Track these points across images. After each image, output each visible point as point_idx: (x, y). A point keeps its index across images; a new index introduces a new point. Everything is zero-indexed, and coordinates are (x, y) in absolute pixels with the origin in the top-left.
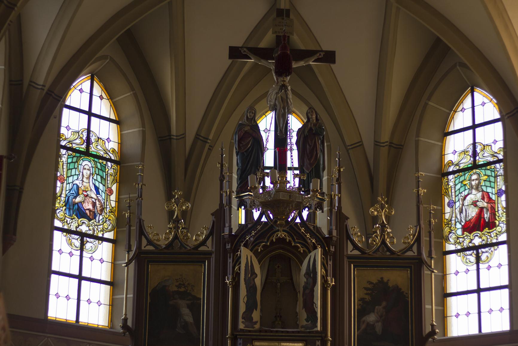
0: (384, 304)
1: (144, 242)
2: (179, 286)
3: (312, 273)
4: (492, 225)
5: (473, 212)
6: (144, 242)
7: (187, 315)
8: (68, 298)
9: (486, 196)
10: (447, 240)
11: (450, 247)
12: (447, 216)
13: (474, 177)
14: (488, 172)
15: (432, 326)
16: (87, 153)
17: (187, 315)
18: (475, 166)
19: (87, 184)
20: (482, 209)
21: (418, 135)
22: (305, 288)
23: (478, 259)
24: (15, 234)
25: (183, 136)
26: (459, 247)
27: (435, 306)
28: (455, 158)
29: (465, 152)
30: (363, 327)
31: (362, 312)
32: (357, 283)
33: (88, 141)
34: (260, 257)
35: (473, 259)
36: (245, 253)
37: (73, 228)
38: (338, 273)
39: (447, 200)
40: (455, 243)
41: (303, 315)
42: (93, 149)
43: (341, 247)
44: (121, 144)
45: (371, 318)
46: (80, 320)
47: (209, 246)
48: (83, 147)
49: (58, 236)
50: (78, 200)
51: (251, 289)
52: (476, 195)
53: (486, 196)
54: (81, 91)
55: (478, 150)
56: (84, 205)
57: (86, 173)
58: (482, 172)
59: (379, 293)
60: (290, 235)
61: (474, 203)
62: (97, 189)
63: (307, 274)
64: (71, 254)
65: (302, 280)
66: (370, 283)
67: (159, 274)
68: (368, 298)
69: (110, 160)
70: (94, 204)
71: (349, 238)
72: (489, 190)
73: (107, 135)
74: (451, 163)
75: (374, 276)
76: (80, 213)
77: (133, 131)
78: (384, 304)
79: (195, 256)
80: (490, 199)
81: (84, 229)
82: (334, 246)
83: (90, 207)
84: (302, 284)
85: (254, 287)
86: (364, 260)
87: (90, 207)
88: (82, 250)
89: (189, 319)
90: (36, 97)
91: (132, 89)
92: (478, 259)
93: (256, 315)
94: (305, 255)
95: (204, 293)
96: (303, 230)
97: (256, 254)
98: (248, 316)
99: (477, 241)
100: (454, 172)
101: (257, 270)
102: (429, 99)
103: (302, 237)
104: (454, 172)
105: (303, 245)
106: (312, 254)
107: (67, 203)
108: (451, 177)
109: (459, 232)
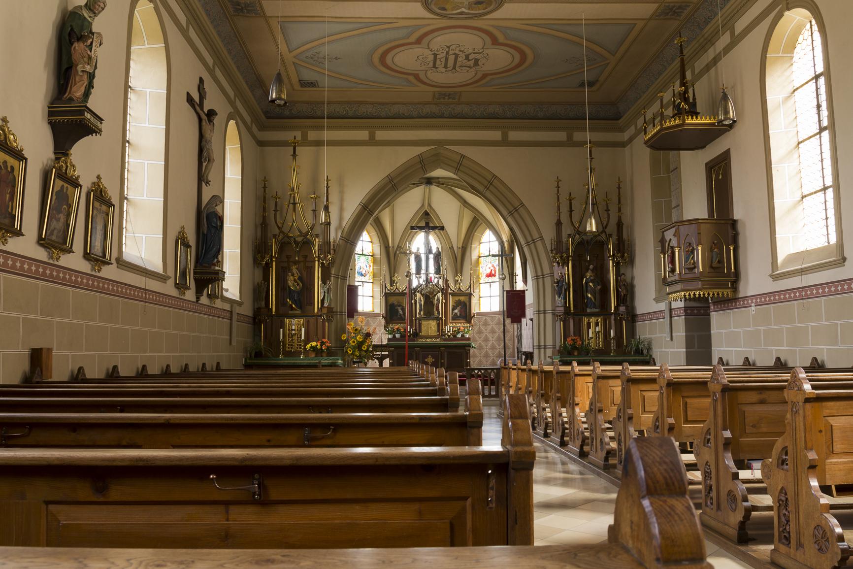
3: (438, 300)
4: (494, 276)
5: (489, 271)
7: (401, 312)
17: (401, 312)
19: (363, 265)
25: (393, 247)
27: (773, 535)
31: (453, 309)
32: (451, 301)
36: (418, 295)
38: (446, 299)
43: (447, 290)
45: (456, 311)
47: (407, 291)
51: (421, 305)
52: (490, 265)
56: (76, 45)
59: (458, 304)
67: (393, 300)
75: (457, 298)
76: (362, 275)
79: (403, 294)
82: (444, 291)
86: (453, 294)
98: (420, 314)
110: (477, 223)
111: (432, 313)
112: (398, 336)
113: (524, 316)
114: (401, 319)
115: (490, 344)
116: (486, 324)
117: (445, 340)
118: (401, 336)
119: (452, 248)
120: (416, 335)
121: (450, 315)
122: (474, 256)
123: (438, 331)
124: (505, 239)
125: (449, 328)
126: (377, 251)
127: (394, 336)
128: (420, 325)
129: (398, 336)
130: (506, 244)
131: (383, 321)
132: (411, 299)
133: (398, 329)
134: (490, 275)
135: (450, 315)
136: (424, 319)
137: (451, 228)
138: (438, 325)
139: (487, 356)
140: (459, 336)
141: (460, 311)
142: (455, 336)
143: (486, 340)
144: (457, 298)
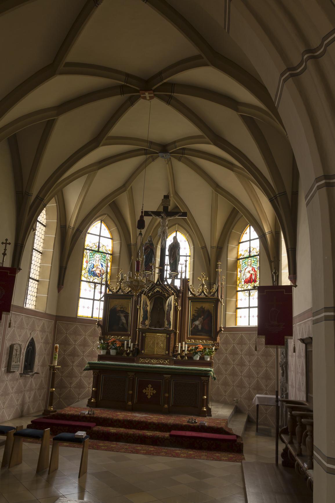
0: (202, 317)
1: (108, 290)
2: (121, 308)
3: (170, 305)
4: (255, 281)
5: (248, 275)
6: (108, 290)
7: (124, 320)
8: (88, 308)
9: (253, 269)
10: (239, 286)
11: (239, 289)
12: (239, 276)
13: (250, 261)
14: (255, 259)
15: (221, 327)
16: (98, 251)
17: (124, 320)
18: (250, 256)
19: (98, 263)
20: (252, 274)
21: (228, 244)
22: (167, 311)
23: (249, 294)
24: (63, 285)
25: (136, 244)
26: (243, 289)
28: (243, 253)
29: (246, 251)
30: (193, 326)
31: (193, 320)
32: (190, 309)
33: (99, 247)
34: (150, 298)
35: (248, 294)
37: (91, 281)
38: (183, 305)
39: (239, 270)
40: (241, 288)
41: (166, 323)
42: (101, 250)
44: (113, 247)
45: (197, 323)
46: (94, 316)
48: (97, 249)
49: (83, 284)
50: (94, 269)
51: (145, 312)
52: (250, 269)
53: (253, 269)
54: (96, 227)
55: (251, 250)
57: (97, 259)
58: (252, 259)
60: (162, 290)
61: (249, 272)
62: (102, 265)
63: (168, 305)
64: (90, 291)
65: (166, 308)
66: (197, 308)
67: (116, 303)
68: (196, 314)
69: (108, 254)
70: (100, 271)
71: (189, 290)
72: (255, 267)
73: (108, 245)
74: (241, 255)
75: (199, 305)
76: (94, 274)
77: (117, 242)
78: (202, 317)
80: (255, 270)
81: (96, 281)
83: (99, 272)
84: (166, 310)
85: (147, 311)
86: (195, 299)
87: (99, 272)
88: (95, 288)
89: (124, 321)
90: (70, 233)
91: (116, 226)
92: (249, 294)
93: (147, 322)
94: (168, 297)
95: (130, 310)
96: (168, 287)
97: (148, 297)
98: (143, 323)
99: (249, 287)
100: (242, 259)
101: (148, 303)
102: (232, 229)
103: (167, 291)
104: (242, 259)
105: (167, 294)
106: (170, 298)
107: (89, 271)
108: (241, 260)
109: (243, 283)
110: (237, 217)
111: (162, 325)
112: (113, 352)
113: (291, 334)
114: (123, 330)
115: (246, 370)
116: (241, 342)
117: (176, 363)
118: (117, 353)
119: (204, 248)
120: (137, 353)
121: (188, 327)
122: (231, 257)
123: (168, 348)
124: (266, 230)
125: (184, 347)
126: (117, 249)
127: (108, 353)
128: (143, 339)
129: (113, 352)
130: (268, 236)
131: (99, 331)
132: (137, 303)
133: (113, 343)
134: (249, 281)
135: (188, 327)
136: (149, 331)
137: (204, 224)
138: (168, 340)
139: (241, 385)
140: (197, 358)
141: (203, 324)
142: (190, 357)
143: (242, 364)
144: (199, 305)
